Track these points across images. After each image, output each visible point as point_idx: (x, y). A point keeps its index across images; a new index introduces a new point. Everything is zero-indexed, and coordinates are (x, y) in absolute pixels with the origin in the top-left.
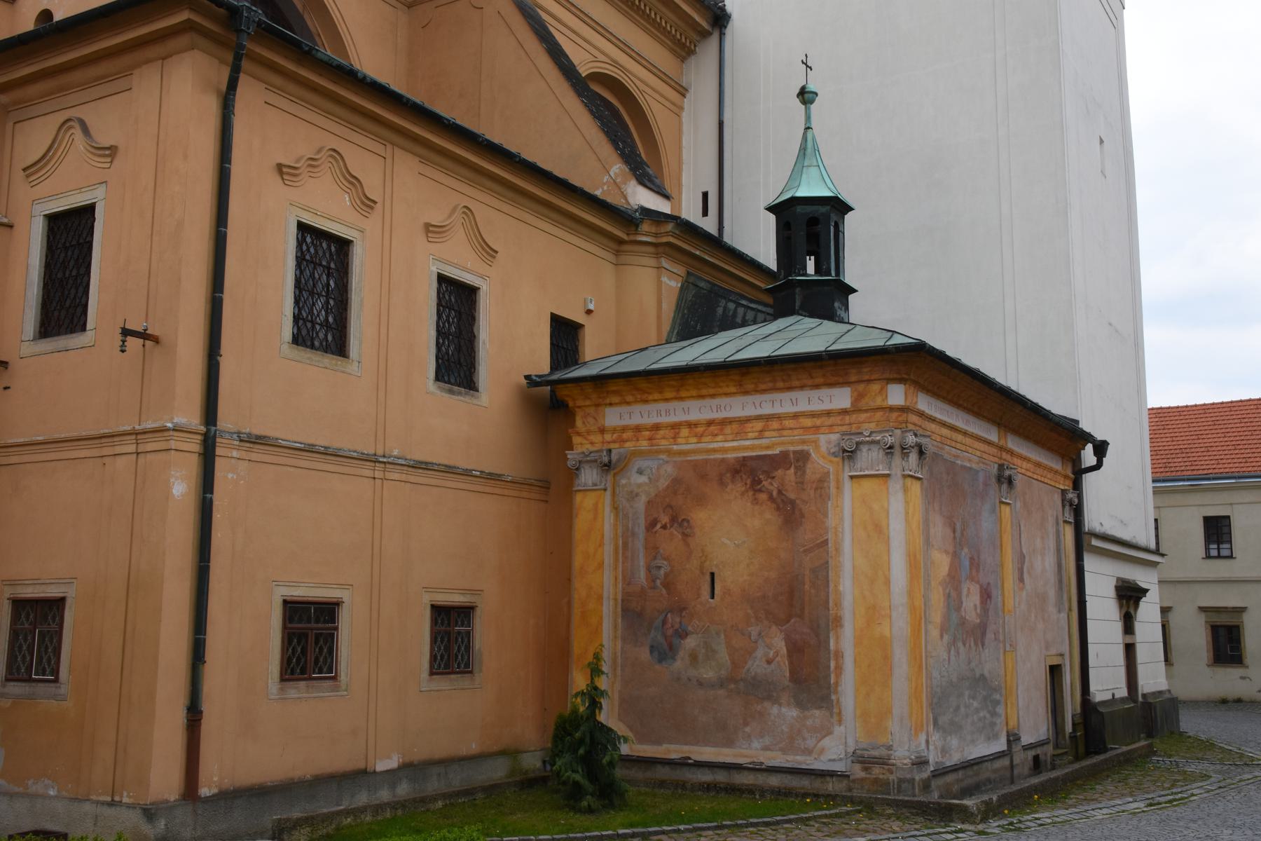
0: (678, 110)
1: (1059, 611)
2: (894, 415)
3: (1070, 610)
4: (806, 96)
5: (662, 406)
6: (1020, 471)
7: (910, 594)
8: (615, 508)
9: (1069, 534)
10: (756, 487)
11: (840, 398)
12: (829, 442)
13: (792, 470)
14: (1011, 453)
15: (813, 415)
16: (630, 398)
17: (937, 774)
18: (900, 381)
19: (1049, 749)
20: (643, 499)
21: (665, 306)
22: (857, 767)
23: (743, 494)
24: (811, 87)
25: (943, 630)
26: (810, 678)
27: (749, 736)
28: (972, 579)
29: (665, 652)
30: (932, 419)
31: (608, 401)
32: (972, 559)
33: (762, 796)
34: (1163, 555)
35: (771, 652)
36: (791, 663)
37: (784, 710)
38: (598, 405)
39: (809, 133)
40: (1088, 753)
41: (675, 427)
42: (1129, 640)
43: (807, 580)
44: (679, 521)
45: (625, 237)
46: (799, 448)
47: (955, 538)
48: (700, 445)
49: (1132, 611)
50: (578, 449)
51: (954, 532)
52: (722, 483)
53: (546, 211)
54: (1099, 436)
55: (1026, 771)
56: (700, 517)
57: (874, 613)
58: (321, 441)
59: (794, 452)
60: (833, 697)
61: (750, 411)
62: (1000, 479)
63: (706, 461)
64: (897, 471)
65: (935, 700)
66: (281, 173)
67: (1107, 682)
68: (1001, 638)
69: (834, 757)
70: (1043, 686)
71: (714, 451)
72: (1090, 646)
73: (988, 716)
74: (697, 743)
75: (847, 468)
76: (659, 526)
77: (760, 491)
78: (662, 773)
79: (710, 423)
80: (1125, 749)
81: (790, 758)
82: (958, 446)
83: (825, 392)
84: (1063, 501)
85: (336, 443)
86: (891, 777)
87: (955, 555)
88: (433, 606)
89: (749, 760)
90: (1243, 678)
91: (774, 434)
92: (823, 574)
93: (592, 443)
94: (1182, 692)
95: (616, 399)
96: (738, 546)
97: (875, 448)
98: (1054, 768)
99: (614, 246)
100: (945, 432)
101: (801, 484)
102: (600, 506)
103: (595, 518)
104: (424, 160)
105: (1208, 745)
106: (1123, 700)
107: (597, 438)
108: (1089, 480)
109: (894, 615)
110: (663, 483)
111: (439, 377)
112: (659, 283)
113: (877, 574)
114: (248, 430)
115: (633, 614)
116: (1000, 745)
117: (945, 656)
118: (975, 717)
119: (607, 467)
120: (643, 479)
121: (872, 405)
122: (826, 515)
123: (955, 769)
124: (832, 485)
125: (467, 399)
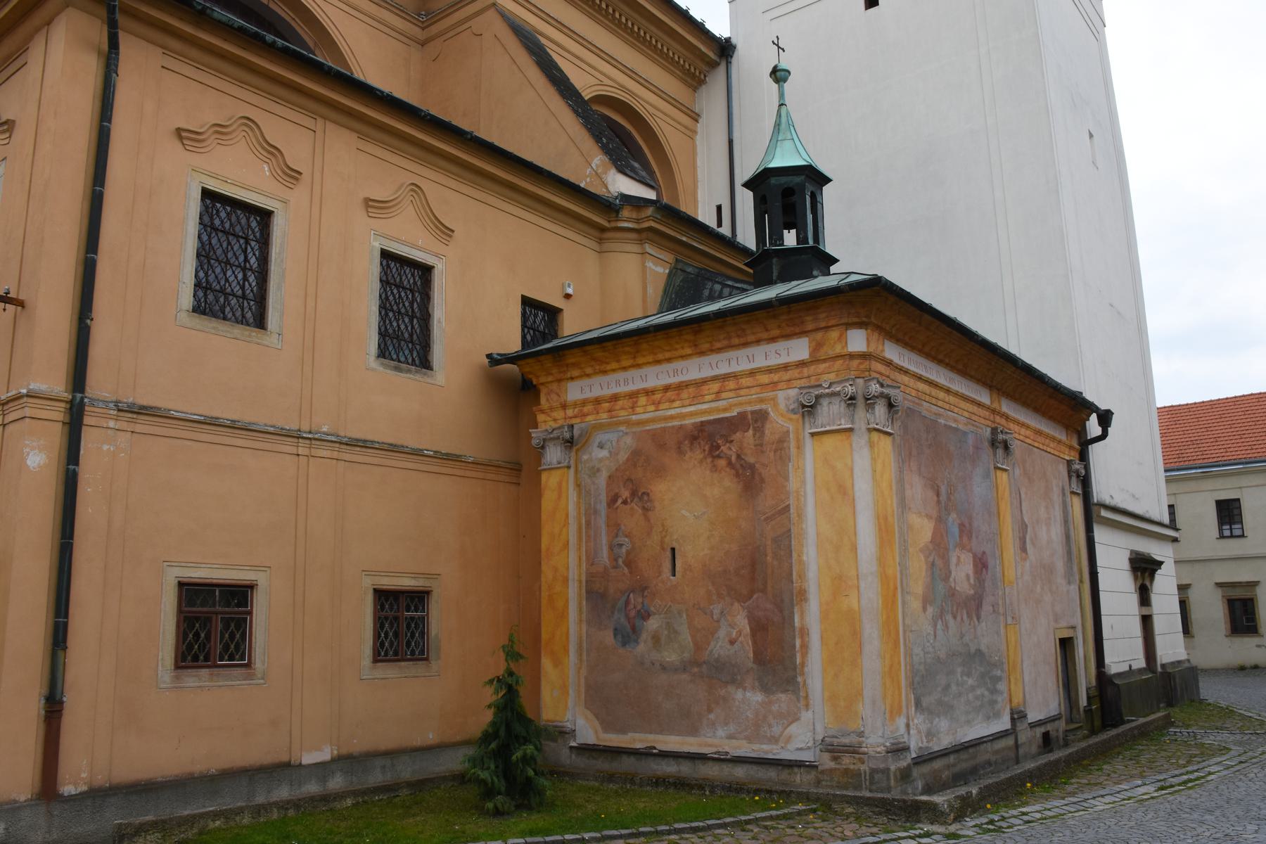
0: (691, 134)
1: (1069, 583)
2: (855, 363)
3: (1081, 581)
4: (779, 75)
5: (621, 376)
6: (1018, 438)
7: (881, 561)
8: (578, 486)
9: (1077, 506)
10: (714, 452)
11: (799, 349)
12: (788, 399)
13: (751, 432)
14: (1007, 418)
15: (770, 370)
16: (589, 370)
17: (918, 761)
18: (860, 325)
19: (1062, 725)
20: (604, 474)
21: (650, 290)
22: (826, 756)
23: (701, 462)
24: (783, 65)
25: (926, 601)
26: (775, 660)
27: (713, 724)
28: (963, 547)
29: (628, 635)
30: (906, 372)
31: (569, 375)
32: (962, 525)
33: (712, 792)
34: (1177, 530)
35: (733, 632)
36: (755, 642)
37: (748, 694)
38: (560, 381)
39: (783, 109)
40: (1105, 726)
41: (633, 395)
42: (1145, 611)
43: (769, 552)
44: (640, 496)
45: (606, 224)
46: (757, 407)
47: (939, 502)
48: (658, 413)
49: (1148, 583)
50: (542, 427)
51: (938, 495)
52: (680, 451)
53: (515, 196)
54: (1103, 407)
55: (1034, 749)
56: (661, 490)
57: (840, 584)
58: (227, 414)
59: (753, 412)
60: (800, 679)
61: (707, 373)
62: (993, 443)
63: (664, 429)
64: (860, 425)
65: (917, 679)
66: (181, 138)
67: (1123, 653)
68: (1001, 610)
69: (803, 745)
70: (1052, 659)
71: (672, 417)
72: (1103, 618)
73: (986, 693)
74: (661, 732)
75: (807, 425)
76: (620, 501)
77: (719, 457)
78: (627, 764)
79: (667, 388)
80: (1142, 720)
81: (756, 747)
82: (940, 403)
83: (781, 345)
84: (1069, 472)
85: (247, 416)
86: (863, 767)
87: (940, 521)
88: (375, 591)
89: (714, 750)
90: (1258, 646)
91: (731, 394)
92: (785, 542)
93: (555, 420)
94: (1203, 659)
95: (576, 373)
96: (696, 517)
97: (836, 400)
98: (1066, 745)
99: (597, 234)
100: (921, 386)
101: (760, 446)
102: (564, 484)
103: (559, 497)
104: (362, 136)
105: (1228, 713)
106: (1140, 671)
107: (559, 414)
108: (1095, 451)
109: (862, 585)
110: (623, 456)
111: (383, 353)
112: (644, 269)
113: (844, 541)
114: (131, 400)
115: (597, 596)
116: (1004, 723)
117: (930, 629)
118: (971, 696)
119: (570, 443)
120: (603, 454)
121: (831, 353)
122: (787, 479)
123: (944, 753)
124: (793, 444)
125: (418, 377)
